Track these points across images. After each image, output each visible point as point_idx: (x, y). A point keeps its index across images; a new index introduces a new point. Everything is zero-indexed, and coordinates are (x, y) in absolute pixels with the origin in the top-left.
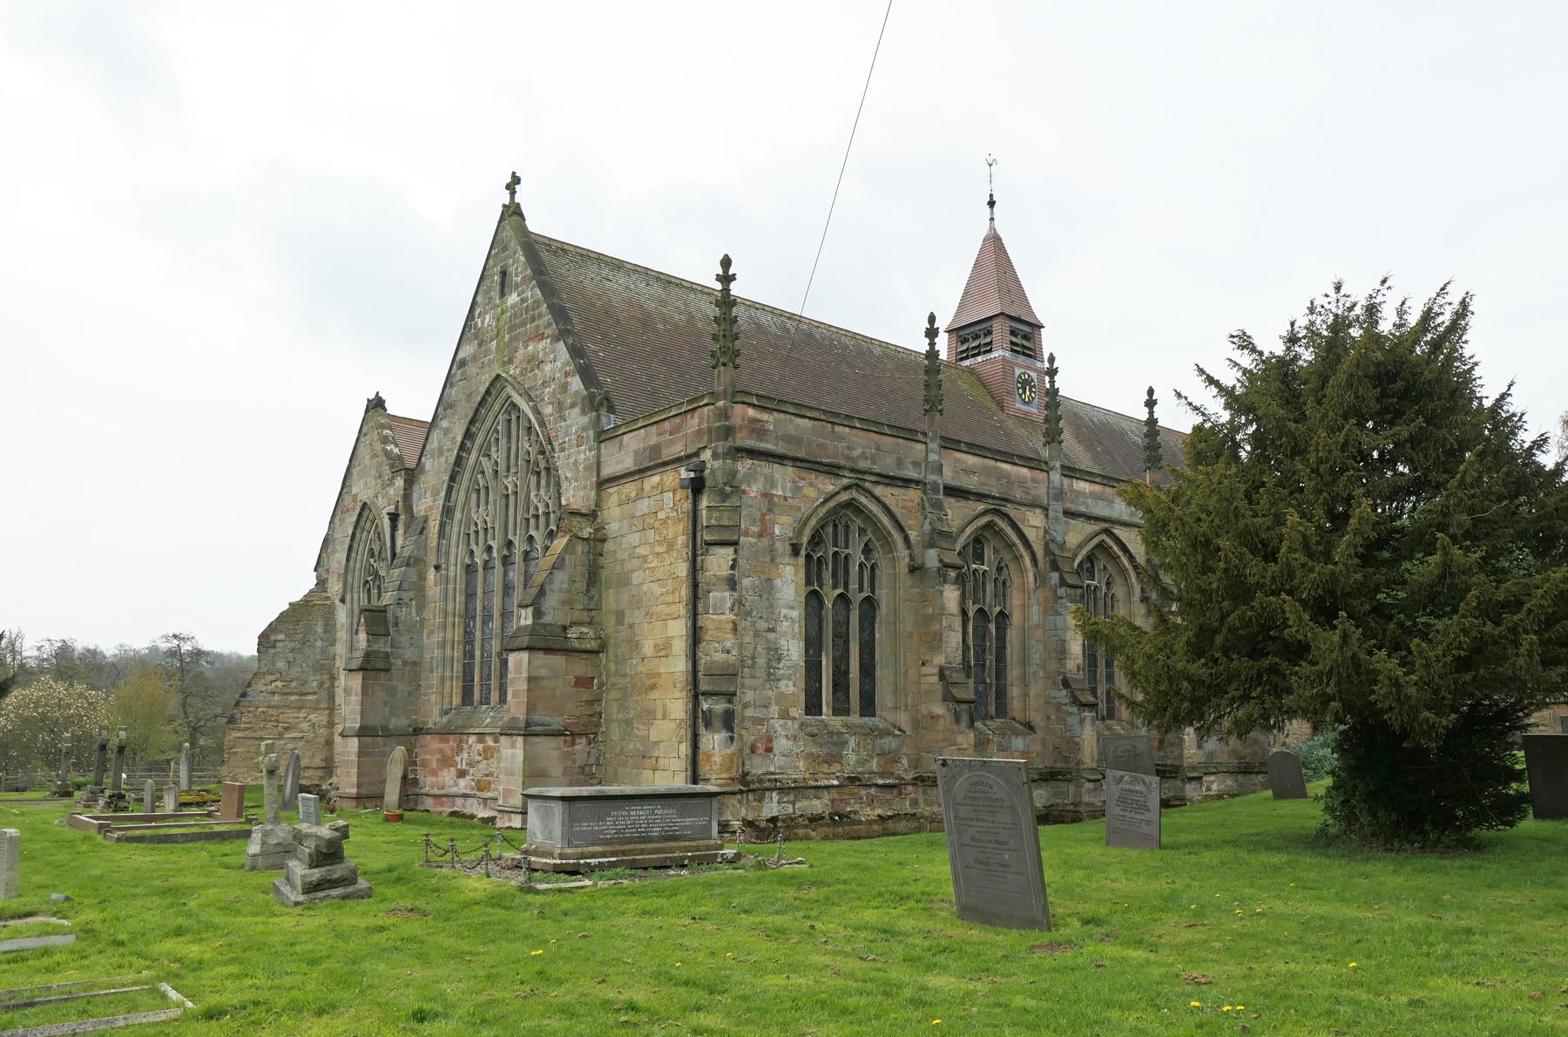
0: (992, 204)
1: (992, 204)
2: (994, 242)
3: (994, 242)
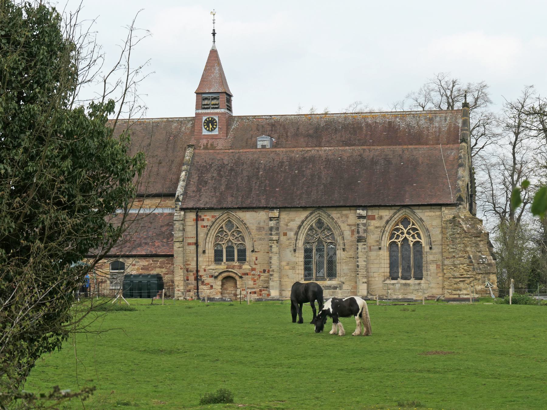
0: (214, 34)
1: (214, 34)
2: (214, 55)
3: (214, 55)
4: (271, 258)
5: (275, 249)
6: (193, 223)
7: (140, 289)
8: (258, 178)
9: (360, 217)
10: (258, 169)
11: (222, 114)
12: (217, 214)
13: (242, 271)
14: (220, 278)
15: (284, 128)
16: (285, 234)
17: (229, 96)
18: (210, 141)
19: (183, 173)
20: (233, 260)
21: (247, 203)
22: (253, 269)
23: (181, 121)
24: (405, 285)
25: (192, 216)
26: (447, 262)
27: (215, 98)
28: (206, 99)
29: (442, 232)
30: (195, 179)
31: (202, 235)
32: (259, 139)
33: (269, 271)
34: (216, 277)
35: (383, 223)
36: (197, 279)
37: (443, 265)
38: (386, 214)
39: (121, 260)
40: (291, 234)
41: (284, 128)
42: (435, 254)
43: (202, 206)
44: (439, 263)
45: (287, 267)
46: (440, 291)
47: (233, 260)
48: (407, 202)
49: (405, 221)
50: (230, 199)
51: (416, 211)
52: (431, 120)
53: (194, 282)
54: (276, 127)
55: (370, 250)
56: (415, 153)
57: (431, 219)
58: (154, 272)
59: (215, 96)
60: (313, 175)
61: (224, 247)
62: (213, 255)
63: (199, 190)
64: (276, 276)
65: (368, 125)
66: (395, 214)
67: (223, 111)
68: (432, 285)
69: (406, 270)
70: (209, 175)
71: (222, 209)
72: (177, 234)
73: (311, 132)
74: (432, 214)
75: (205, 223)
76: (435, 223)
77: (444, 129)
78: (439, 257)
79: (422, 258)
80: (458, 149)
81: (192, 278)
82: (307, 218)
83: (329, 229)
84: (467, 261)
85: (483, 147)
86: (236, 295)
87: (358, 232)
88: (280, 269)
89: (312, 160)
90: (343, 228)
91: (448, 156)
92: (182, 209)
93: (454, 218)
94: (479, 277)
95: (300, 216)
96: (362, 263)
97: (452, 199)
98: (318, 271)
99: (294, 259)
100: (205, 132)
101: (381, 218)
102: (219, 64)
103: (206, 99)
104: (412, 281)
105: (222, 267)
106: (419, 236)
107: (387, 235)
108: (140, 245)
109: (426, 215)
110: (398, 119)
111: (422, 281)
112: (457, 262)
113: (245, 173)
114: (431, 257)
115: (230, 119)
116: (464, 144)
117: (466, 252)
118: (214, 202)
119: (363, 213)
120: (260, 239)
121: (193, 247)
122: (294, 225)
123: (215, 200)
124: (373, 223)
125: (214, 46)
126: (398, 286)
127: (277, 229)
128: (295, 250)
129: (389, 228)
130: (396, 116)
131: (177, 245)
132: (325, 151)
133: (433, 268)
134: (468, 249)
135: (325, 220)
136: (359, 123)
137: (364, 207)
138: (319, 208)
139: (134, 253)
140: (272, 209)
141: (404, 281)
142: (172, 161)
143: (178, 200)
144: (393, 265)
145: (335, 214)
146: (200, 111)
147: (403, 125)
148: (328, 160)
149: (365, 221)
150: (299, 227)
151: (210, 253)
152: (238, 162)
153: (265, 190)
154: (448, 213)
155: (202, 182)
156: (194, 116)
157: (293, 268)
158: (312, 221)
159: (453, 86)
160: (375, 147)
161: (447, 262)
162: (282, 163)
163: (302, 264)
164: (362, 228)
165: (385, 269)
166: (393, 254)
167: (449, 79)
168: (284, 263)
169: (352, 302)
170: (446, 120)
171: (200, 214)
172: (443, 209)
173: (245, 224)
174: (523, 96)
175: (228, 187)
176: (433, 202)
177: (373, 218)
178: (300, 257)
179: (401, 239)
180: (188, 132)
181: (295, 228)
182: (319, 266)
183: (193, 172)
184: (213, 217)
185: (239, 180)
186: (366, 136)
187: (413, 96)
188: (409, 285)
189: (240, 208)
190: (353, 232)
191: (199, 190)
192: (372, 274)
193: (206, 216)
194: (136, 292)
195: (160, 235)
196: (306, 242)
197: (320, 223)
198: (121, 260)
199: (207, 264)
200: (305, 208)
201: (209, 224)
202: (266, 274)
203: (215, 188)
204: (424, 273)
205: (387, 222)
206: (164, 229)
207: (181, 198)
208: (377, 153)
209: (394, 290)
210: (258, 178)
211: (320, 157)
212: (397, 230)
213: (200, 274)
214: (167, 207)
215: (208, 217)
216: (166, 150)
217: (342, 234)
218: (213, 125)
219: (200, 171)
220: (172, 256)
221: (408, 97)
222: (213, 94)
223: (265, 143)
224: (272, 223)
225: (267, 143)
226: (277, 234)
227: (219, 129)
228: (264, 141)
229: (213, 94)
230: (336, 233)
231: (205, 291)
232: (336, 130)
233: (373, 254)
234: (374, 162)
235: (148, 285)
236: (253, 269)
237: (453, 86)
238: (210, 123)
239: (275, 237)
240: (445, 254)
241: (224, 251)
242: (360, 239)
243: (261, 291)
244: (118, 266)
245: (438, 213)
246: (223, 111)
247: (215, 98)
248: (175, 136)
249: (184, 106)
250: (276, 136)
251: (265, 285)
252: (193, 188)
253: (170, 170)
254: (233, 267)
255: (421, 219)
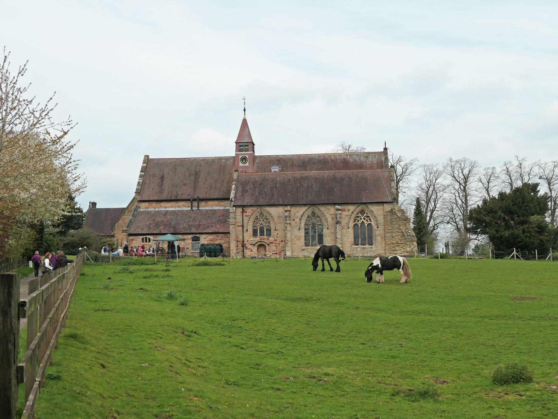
0: (245, 110)
1: (245, 110)
3: (245, 122)
4: (286, 234)
5: (289, 228)
6: (241, 214)
7: (210, 252)
8: (276, 189)
9: (338, 210)
10: (276, 183)
11: (250, 154)
12: (254, 209)
13: (269, 241)
14: (257, 245)
15: (285, 162)
16: (294, 220)
17: (254, 144)
18: (244, 169)
19: (234, 186)
20: (264, 235)
21: (272, 202)
22: (276, 240)
23: (230, 158)
24: (363, 248)
25: (240, 210)
26: (387, 235)
27: (246, 146)
28: (241, 146)
29: (384, 218)
30: (240, 189)
31: (245, 221)
32: (273, 167)
33: (285, 241)
34: (254, 245)
35: (350, 213)
36: (243, 246)
37: (385, 236)
38: (352, 208)
39: (197, 235)
40: (297, 220)
41: (285, 162)
42: (380, 230)
43: (246, 204)
44: (383, 236)
45: (295, 239)
46: (383, 252)
47: (264, 235)
48: (364, 201)
49: (362, 212)
50: (261, 200)
51: (369, 206)
52: (367, 157)
53: (242, 248)
54: (283, 162)
55: (343, 228)
56: (365, 174)
57: (377, 210)
58: (217, 242)
59: (246, 144)
60: (308, 187)
61: (258, 227)
62: (252, 232)
63: (243, 195)
64: (289, 243)
65: (332, 160)
66: (357, 208)
67: (251, 152)
68: (379, 248)
69: (364, 239)
70: (248, 187)
71: (257, 206)
72: (232, 220)
73: (300, 164)
74: (378, 208)
75: (247, 214)
76: (380, 213)
78: (382, 232)
79: (372, 233)
81: (240, 245)
82: (306, 210)
83: (319, 217)
84: (401, 234)
86: (265, 255)
87: (336, 218)
88: (292, 240)
89: (307, 178)
90: (327, 216)
91: (384, 176)
92: (234, 206)
93: (392, 210)
94: (408, 243)
95: (301, 210)
96: (339, 236)
97: (390, 199)
98: (312, 241)
99: (299, 234)
100: (241, 164)
101: (349, 210)
103: (241, 146)
104: (367, 246)
105: (258, 239)
106: (370, 219)
107: (352, 220)
108: (208, 227)
109: (375, 209)
111: (373, 246)
112: (394, 235)
113: (269, 186)
114: (378, 232)
115: (255, 158)
117: (400, 229)
118: (252, 202)
119: (339, 207)
120: (280, 223)
121: (241, 228)
122: (299, 215)
123: (253, 201)
124: (344, 213)
125: (245, 117)
126: (359, 249)
127: (290, 217)
128: (299, 229)
129: (353, 216)
130: (347, 155)
131: (232, 226)
132: (314, 173)
133: (379, 238)
134: (401, 227)
135: (317, 212)
137: (339, 204)
138: (313, 205)
139: (205, 232)
140: (286, 205)
141: (362, 246)
143: (232, 201)
144: (356, 237)
145: (322, 208)
146: (238, 153)
147: (351, 160)
148: (316, 178)
149: (340, 212)
150: (302, 216)
151: (251, 231)
152: (264, 180)
153: (281, 195)
154: (388, 207)
155: (244, 191)
156: (235, 155)
157: (299, 239)
158: (309, 212)
160: (342, 171)
161: (387, 235)
162: (289, 180)
163: (304, 237)
164: (338, 216)
165: (351, 238)
166: (356, 230)
167: (347, 145)
168: (293, 237)
169: (395, 259)
171: (244, 209)
172: (385, 205)
173: (271, 214)
175: (260, 193)
176: (379, 201)
177: (344, 210)
178: (302, 233)
179: (360, 222)
180: (231, 164)
181: (300, 217)
182: (313, 238)
183: (239, 185)
184: (252, 210)
185: (266, 190)
186: (332, 166)
188: (365, 248)
189: (268, 205)
190: (333, 218)
191: (243, 195)
192: (344, 242)
194: (213, 254)
195: (219, 221)
196: (306, 225)
197: (313, 213)
198: (197, 235)
199: (249, 237)
200: (305, 205)
201: (250, 214)
202: (283, 243)
203: (253, 194)
204: (374, 241)
205: (353, 212)
206: (221, 218)
207: (233, 200)
208: (343, 174)
209: (357, 251)
210: (276, 189)
212: (358, 217)
213: (245, 243)
214: (221, 206)
215: (249, 211)
216: (220, 174)
217: (326, 220)
219: (243, 185)
220: (229, 233)
222: (245, 143)
223: (276, 170)
224: (287, 214)
225: (277, 170)
226: (290, 220)
227: (249, 163)
228: (275, 169)
229: (245, 143)
230: (323, 219)
231: (248, 253)
233: (344, 231)
234: (342, 179)
235: (215, 249)
236: (276, 240)
238: (244, 159)
239: (288, 222)
240: (386, 231)
241: (259, 230)
242: (338, 223)
243: (280, 252)
244: (196, 239)
245: (382, 207)
246: (251, 152)
247: (246, 146)
248: (224, 167)
249: (230, 151)
250: (281, 166)
251: (283, 249)
252: (239, 194)
254: (264, 239)
255: (372, 211)
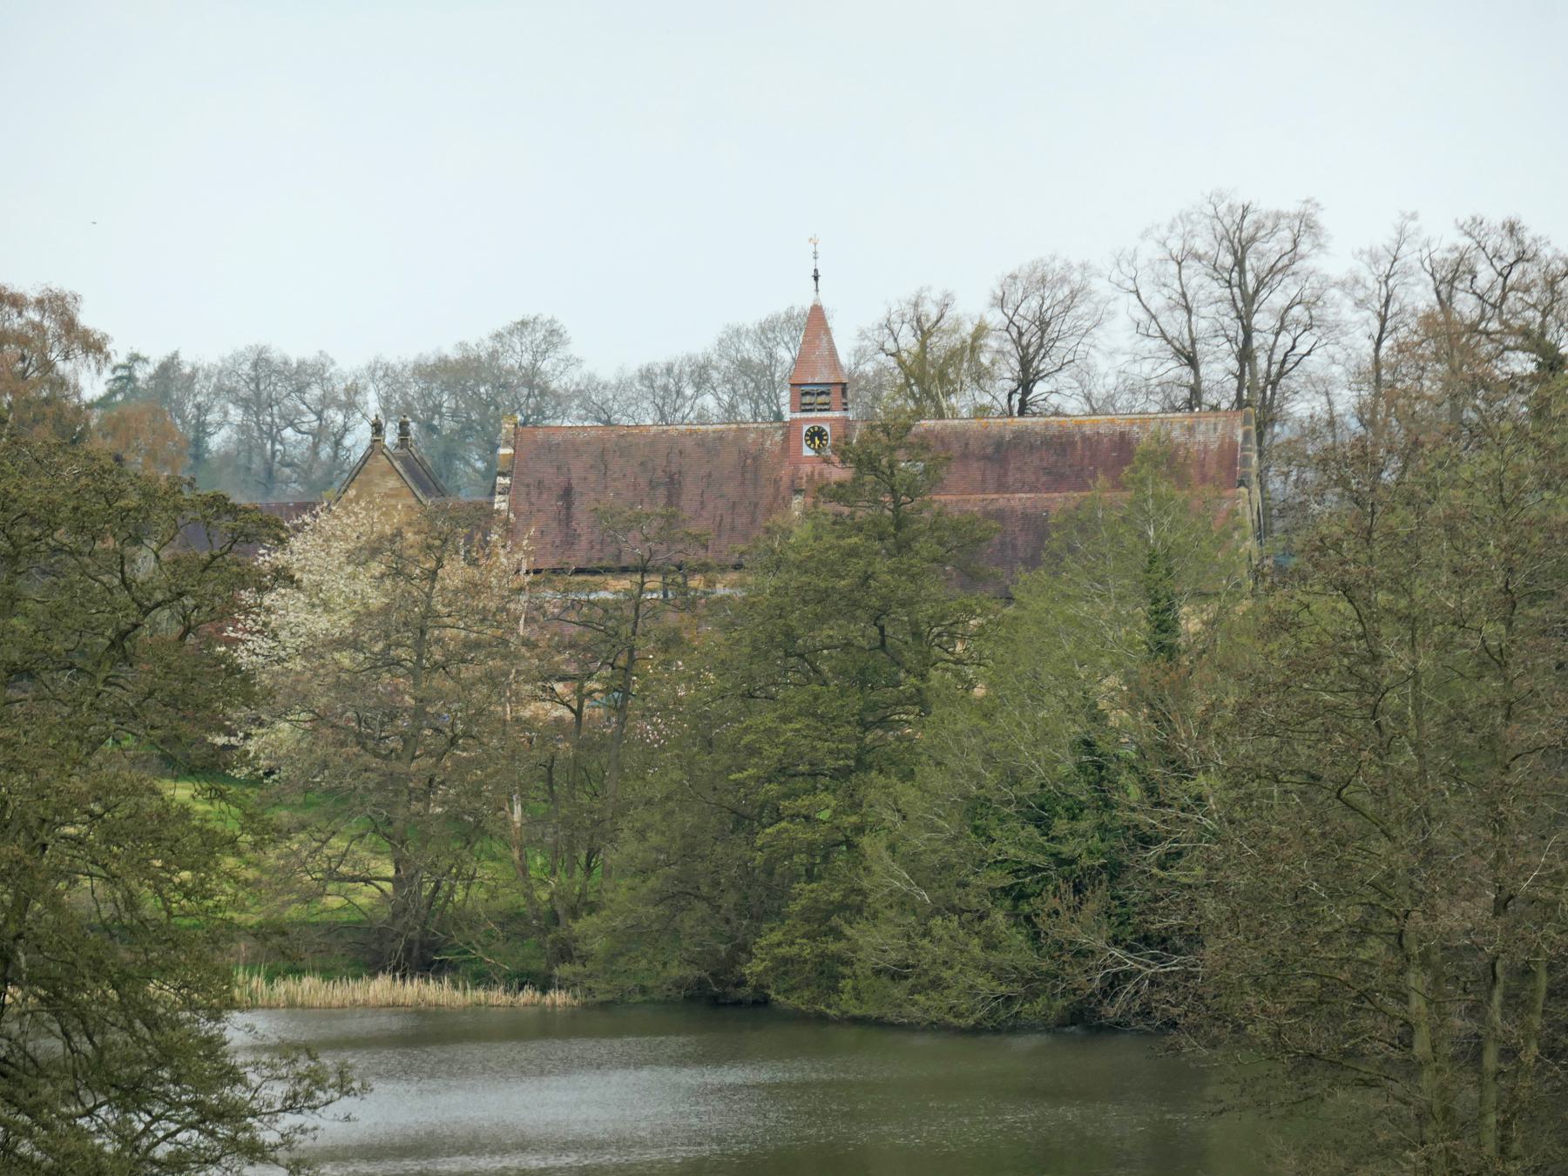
1: (816, 278)
11: (836, 420)
15: (943, 442)
28: (807, 393)
41: (943, 442)
59: (822, 389)
60: (1002, 544)
65: (1086, 439)
67: (837, 414)
73: (989, 450)
77: (1214, 447)
80: (1234, 499)
85: (1309, 353)
89: (1000, 515)
102: (827, 331)
103: (807, 393)
110: (1135, 429)
116: (1242, 489)
136: (1070, 435)
142: (756, 505)
146: (798, 415)
147: (1145, 438)
148: (1025, 516)
159: (1243, 217)
167: (1240, 200)
170: (1215, 429)
174: (1396, 236)
180: (777, 449)
187: (1157, 235)
193: (1153, 826)
211: (1013, 511)
218: (821, 439)
221: (1144, 236)
232: (1032, 447)
237: (1243, 217)
246: (837, 414)
248: (755, 459)
253: (753, 521)
